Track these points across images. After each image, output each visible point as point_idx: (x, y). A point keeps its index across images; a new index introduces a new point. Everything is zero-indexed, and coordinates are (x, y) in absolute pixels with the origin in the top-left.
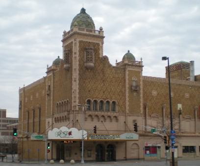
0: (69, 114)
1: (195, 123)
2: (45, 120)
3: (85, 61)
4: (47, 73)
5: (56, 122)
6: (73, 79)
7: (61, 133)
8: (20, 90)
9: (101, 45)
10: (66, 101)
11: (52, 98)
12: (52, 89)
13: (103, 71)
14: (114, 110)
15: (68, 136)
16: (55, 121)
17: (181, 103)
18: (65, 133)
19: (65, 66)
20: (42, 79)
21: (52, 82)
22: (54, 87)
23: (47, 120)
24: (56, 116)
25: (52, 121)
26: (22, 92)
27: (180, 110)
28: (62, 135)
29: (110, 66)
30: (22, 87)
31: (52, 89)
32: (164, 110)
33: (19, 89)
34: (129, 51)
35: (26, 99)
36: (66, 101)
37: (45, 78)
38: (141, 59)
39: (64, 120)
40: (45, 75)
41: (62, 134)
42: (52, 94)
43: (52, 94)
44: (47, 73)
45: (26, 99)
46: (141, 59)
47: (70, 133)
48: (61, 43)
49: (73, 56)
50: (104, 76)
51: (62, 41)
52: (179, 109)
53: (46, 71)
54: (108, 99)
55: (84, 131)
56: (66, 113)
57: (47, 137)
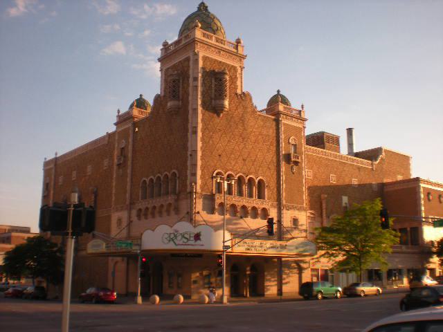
0: (177, 200)
1: (174, 242)
2: (109, 218)
3: (213, 96)
4: (116, 124)
5: (139, 219)
6: (190, 131)
7: (175, 236)
8: (47, 164)
9: (239, 71)
10: (147, 181)
11: (129, 171)
12: (130, 155)
13: (242, 120)
14: (261, 196)
15: (192, 242)
16: (139, 216)
17: (346, 195)
18: (186, 236)
19: (169, 104)
20: (104, 137)
21: (130, 140)
22: (134, 151)
23: (115, 217)
24: (142, 205)
25: (130, 217)
26: (52, 166)
27: (346, 207)
28: (179, 240)
29: (254, 110)
30: (51, 156)
31: (130, 155)
32: (324, 205)
33: (44, 160)
34: (278, 91)
35: (61, 179)
36: (147, 181)
37: (110, 135)
38: (302, 107)
39: (165, 214)
40: (113, 129)
41: (179, 238)
42: (129, 163)
43: (129, 163)
44: (116, 124)
45: (61, 179)
46: (302, 107)
47: (197, 237)
48: (159, 65)
49: (191, 85)
50: (245, 129)
51: (160, 60)
52: (344, 205)
53: (115, 120)
54: (250, 174)
55: (226, 232)
56: (171, 199)
57: (140, 245)
